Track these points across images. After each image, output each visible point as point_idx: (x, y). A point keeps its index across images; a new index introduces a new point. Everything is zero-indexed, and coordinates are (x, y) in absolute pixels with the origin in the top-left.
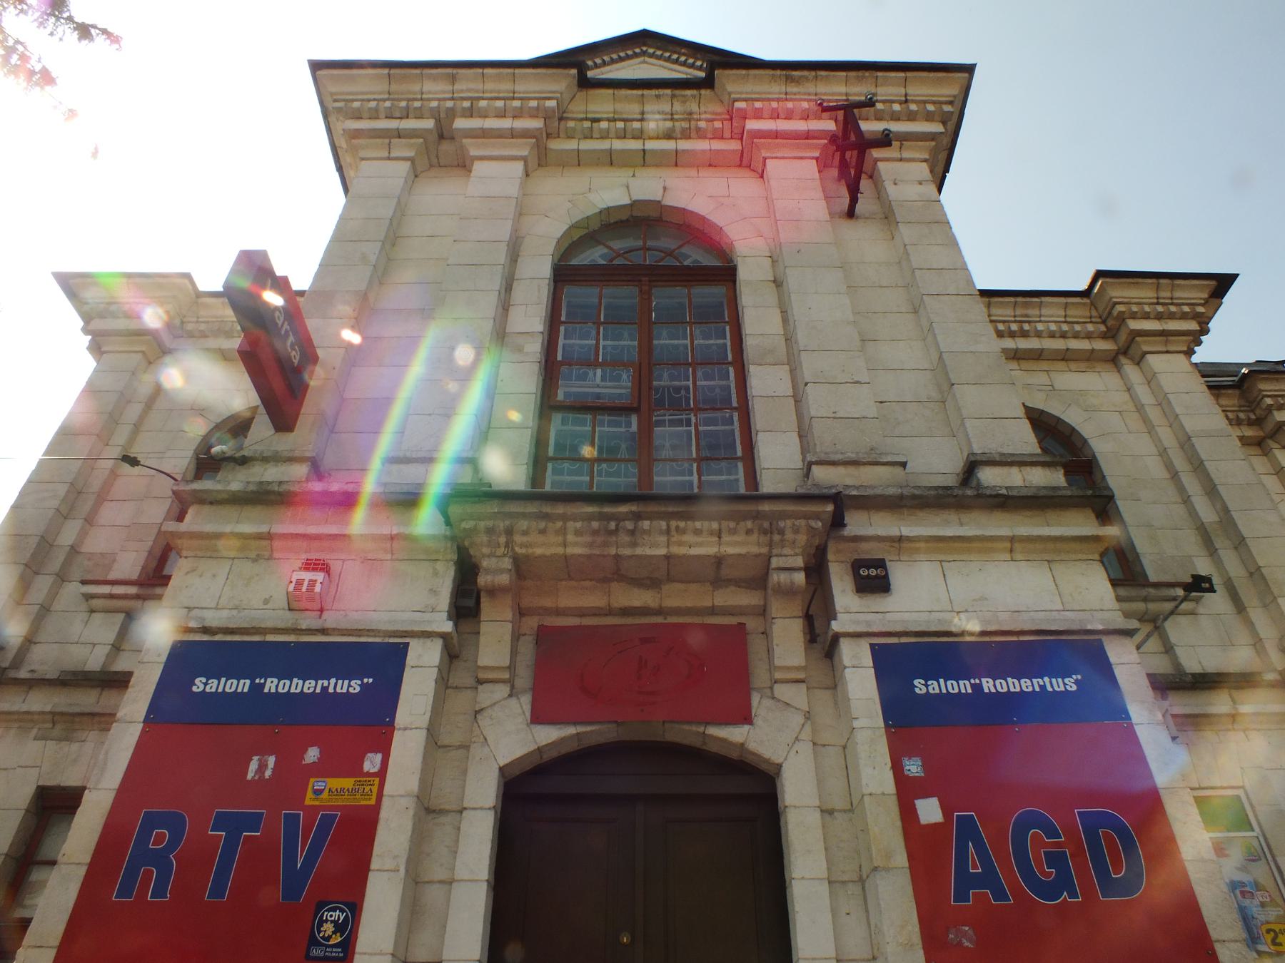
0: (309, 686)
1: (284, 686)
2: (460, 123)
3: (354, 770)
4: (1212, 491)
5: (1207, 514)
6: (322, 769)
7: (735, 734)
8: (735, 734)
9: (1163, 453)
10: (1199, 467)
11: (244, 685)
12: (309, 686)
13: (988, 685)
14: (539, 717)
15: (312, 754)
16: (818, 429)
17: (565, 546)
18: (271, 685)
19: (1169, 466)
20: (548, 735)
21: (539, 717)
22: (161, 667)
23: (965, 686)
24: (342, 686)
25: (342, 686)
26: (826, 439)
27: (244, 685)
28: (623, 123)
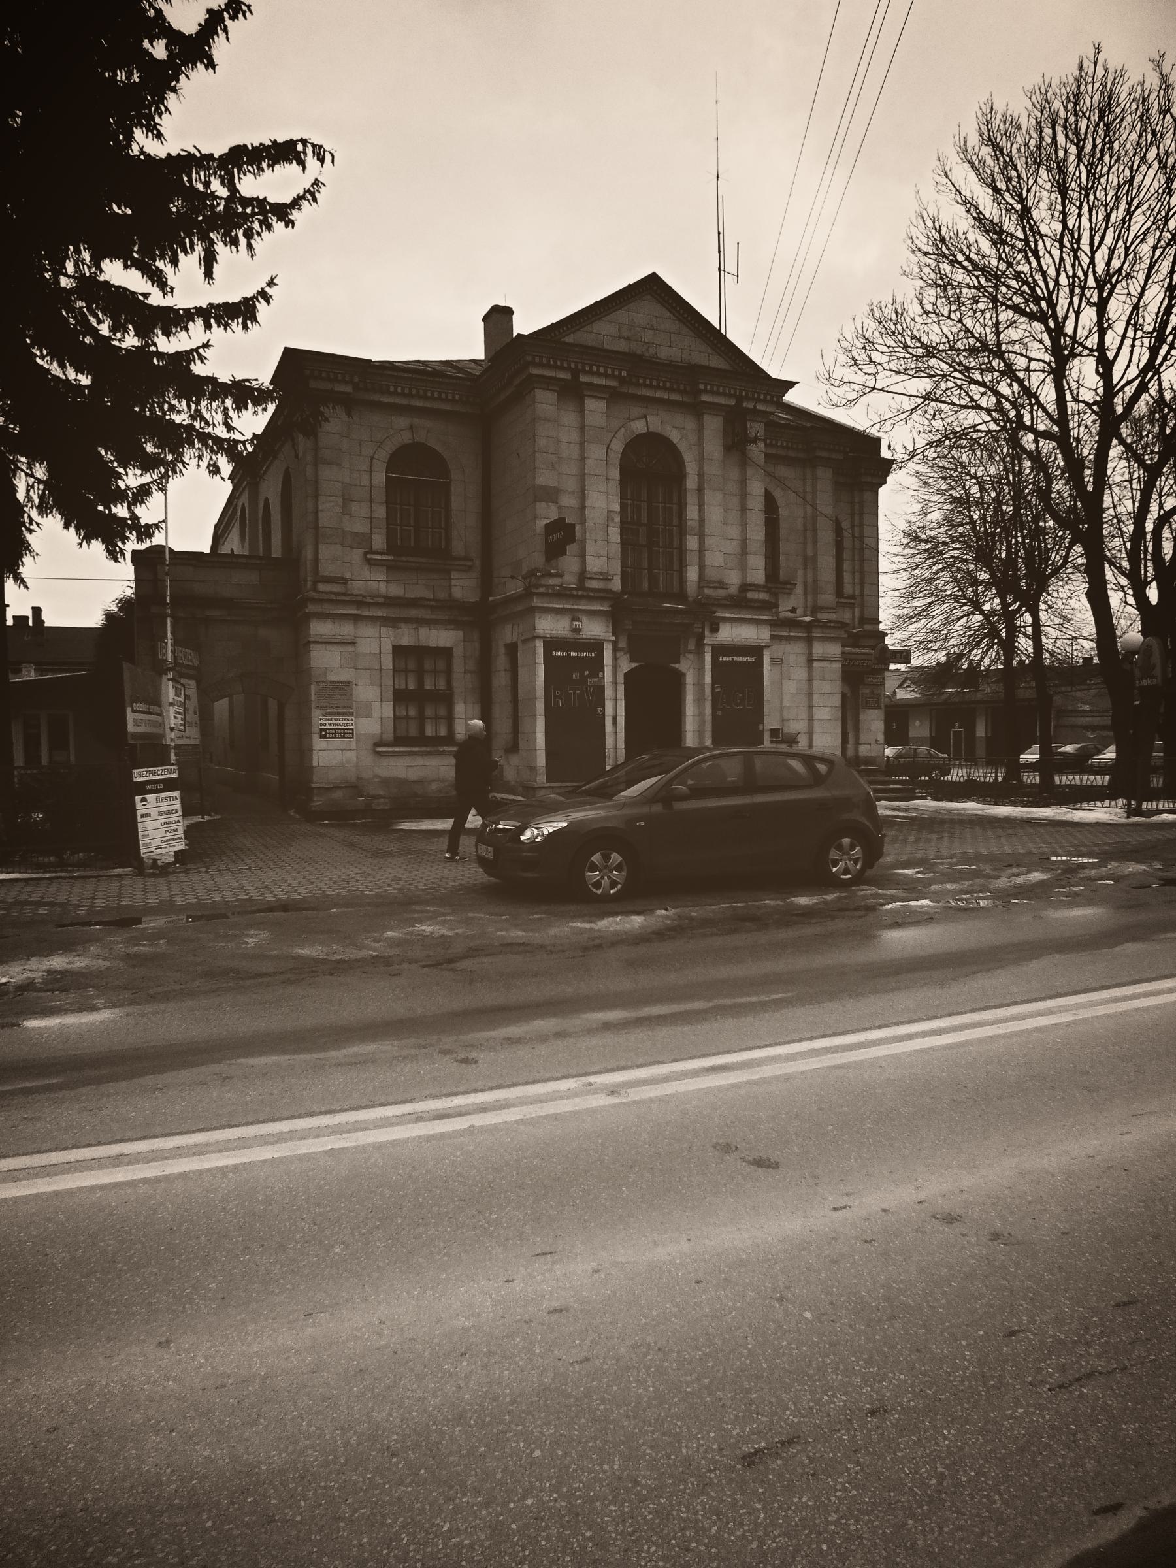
0: (582, 654)
1: (576, 654)
3: (597, 676)
4: (815, 542)
5: (810, 553)
6: (590, 676)
7: (676, 666)
8: (676, 666)
9: (805, 517)
10: (815, 530)
11: (566, 654)
12: (582, 654)
13: (736, 658)
14: (632, 661)
15: (587, 673)
16: (707, 570)
17: (411, 428)
18: (572, 654)
19: (805, 525)
20: (634, 665)
21: (632, 661)
22: (765, 713)
23: (730, 659)
24: (589, 654)
25: (589, 654)
26: (711, 574)
27: (566, 654)
28: (695, 487)
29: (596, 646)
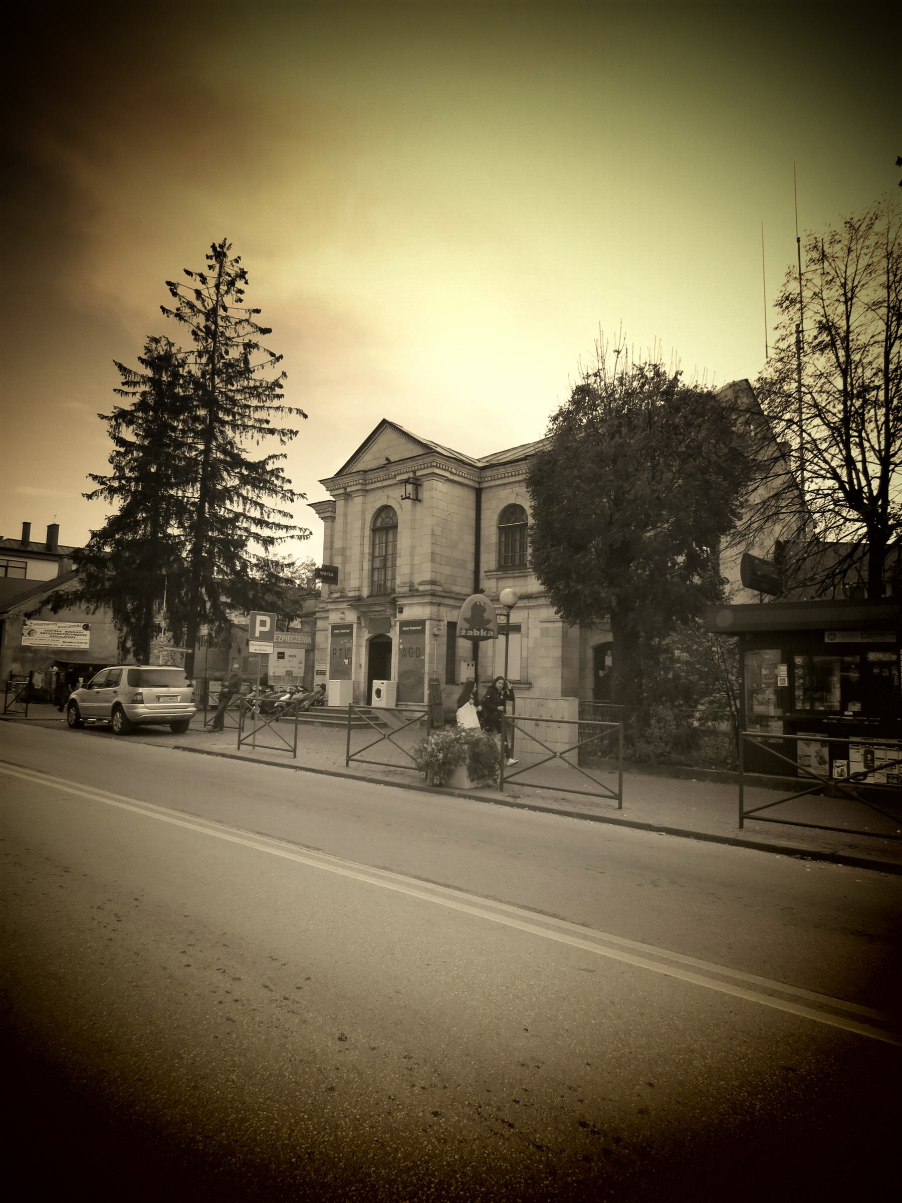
2: (349, 490)
29: (350, 627)
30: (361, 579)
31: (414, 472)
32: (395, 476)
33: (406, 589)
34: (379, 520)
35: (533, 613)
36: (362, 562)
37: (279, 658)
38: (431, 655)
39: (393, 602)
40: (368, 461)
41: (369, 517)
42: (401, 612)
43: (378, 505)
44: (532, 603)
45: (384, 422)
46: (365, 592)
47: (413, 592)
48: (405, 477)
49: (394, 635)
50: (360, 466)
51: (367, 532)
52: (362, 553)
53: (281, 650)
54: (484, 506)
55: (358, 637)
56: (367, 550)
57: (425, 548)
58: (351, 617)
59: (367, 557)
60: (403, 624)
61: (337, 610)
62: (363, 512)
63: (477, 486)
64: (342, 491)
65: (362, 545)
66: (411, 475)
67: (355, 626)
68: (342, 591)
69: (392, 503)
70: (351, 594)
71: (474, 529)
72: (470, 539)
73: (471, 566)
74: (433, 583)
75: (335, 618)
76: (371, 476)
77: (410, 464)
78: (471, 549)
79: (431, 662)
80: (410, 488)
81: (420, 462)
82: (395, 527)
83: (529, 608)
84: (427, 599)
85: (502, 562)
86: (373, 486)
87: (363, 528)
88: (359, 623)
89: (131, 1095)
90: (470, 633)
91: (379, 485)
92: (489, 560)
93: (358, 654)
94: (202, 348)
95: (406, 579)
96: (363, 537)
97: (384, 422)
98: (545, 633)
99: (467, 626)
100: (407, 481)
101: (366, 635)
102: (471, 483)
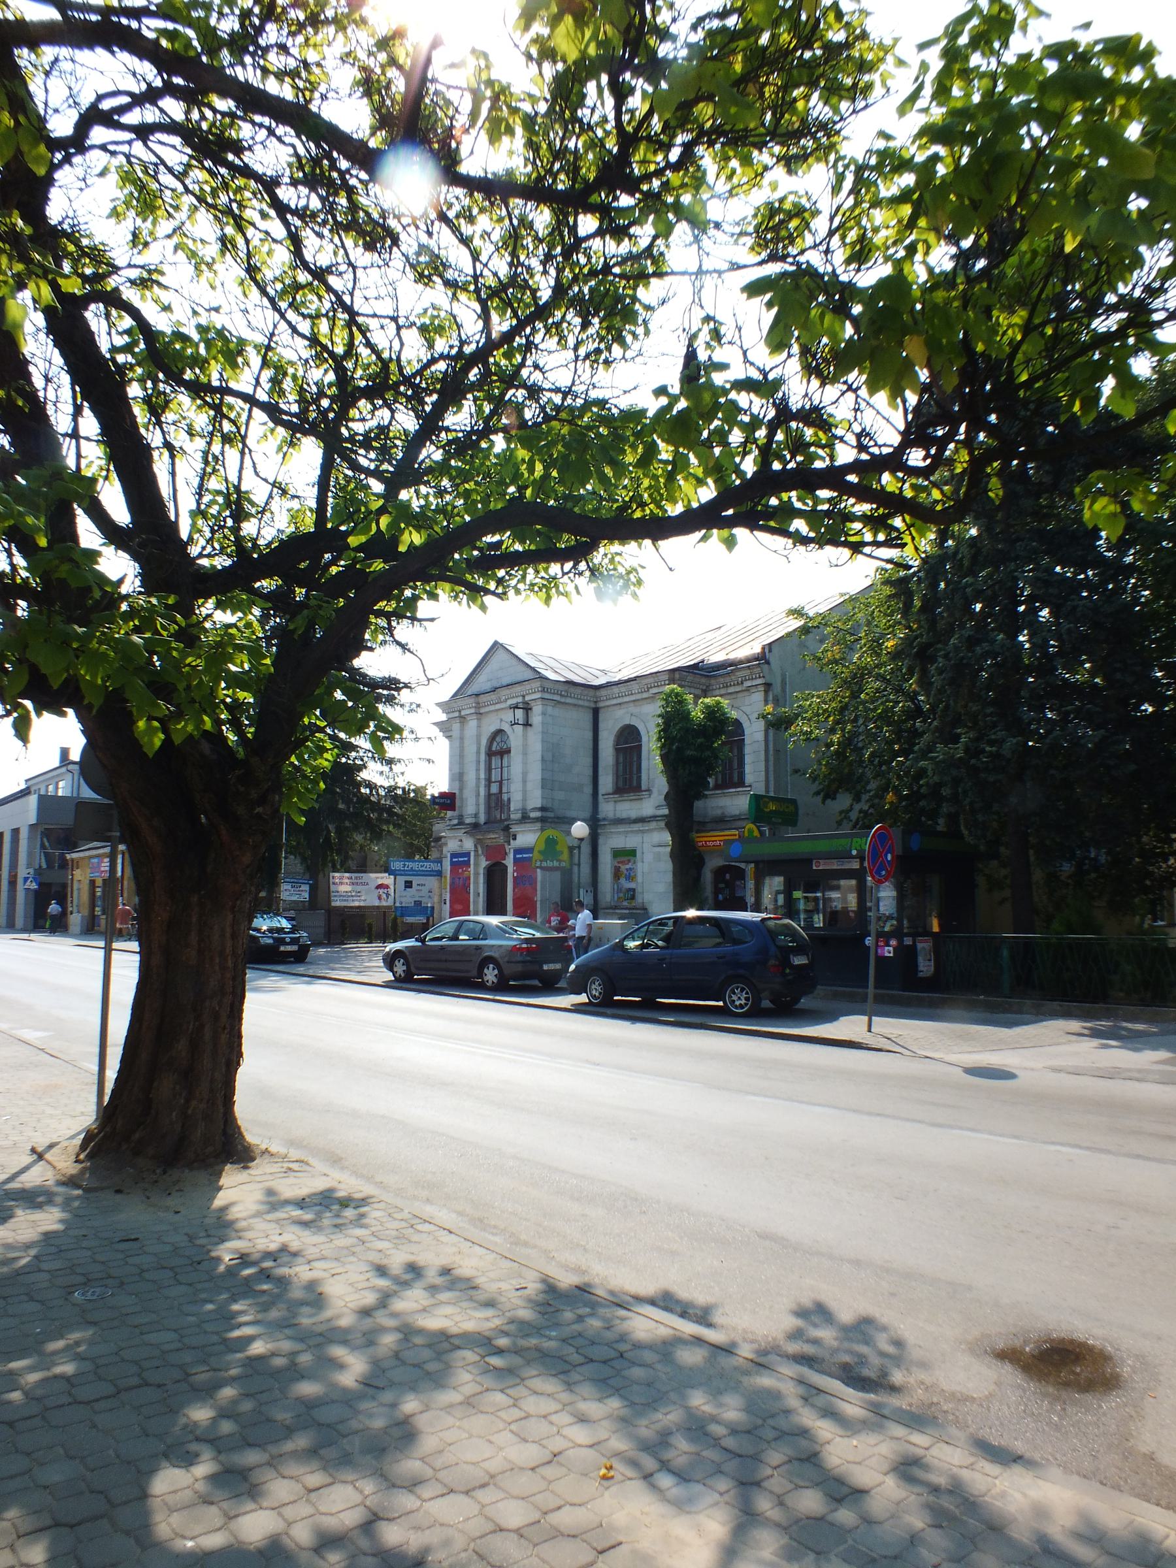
2: (463, 713)
29: (468, 854)
30: (478, 805)
31: (524, 696)
32: (506, 700)
33: (519, 816)
34: (495, 744)
35: (647, 837)
36: (478, 786)
37: (406, 887)
38: (542, 882)
39: (507, 829)
40: (482, 683)
41: (484, 742)
42: (515, 839)
43: (493, 729)
44: (646, 827)
45: (496, 643)
46: (482, 819)
47: (525, 818)
48: (514, 701)
49: (509, 862)
50: (474, 688)
51: (483, 757)
52: (478, 779)
53: (409, 878)
54: (601, 725)
55: (477, 865)
56: (482, 776)
57: (535, 775)
58: (469, 844)
59: (483, 783)
60: (518, 851)
61: (455, 837)
62: (479, 737)
63: (593, 705)
64: (457, 714)
65: (478, 770)
66: (520, 700)
67: (472, 854)
68: (461, 817)
69: (506, 727)
70: (468, 821)
71: (591, 752)
72: (588, 761)
73: (588, 790)
74: (542, 809)
75: (452, 846)
76: (483, 698)
77: (518, 688)
78: (589, 772)
79: (543, 888)
80: (520, 714)
81: (528, 687)
82: (508, 751)
83: (643, 832)
84: (538, 825)
85: (621, 784)
86: (487, 709)
87: (478, 752)
88: (476, 851)
89: (290, 788)
90: (544, 864)
91: (492, 708)
92: (607, 782)
93: (476, 883)
94: (349, 31)
95: (520, 806)
96: (478, 762)
97: (496, 643)
98: (658, 858)
99: (542, 858)
100: (516, 707)
101: (484, 863)
102: (586, 704)
